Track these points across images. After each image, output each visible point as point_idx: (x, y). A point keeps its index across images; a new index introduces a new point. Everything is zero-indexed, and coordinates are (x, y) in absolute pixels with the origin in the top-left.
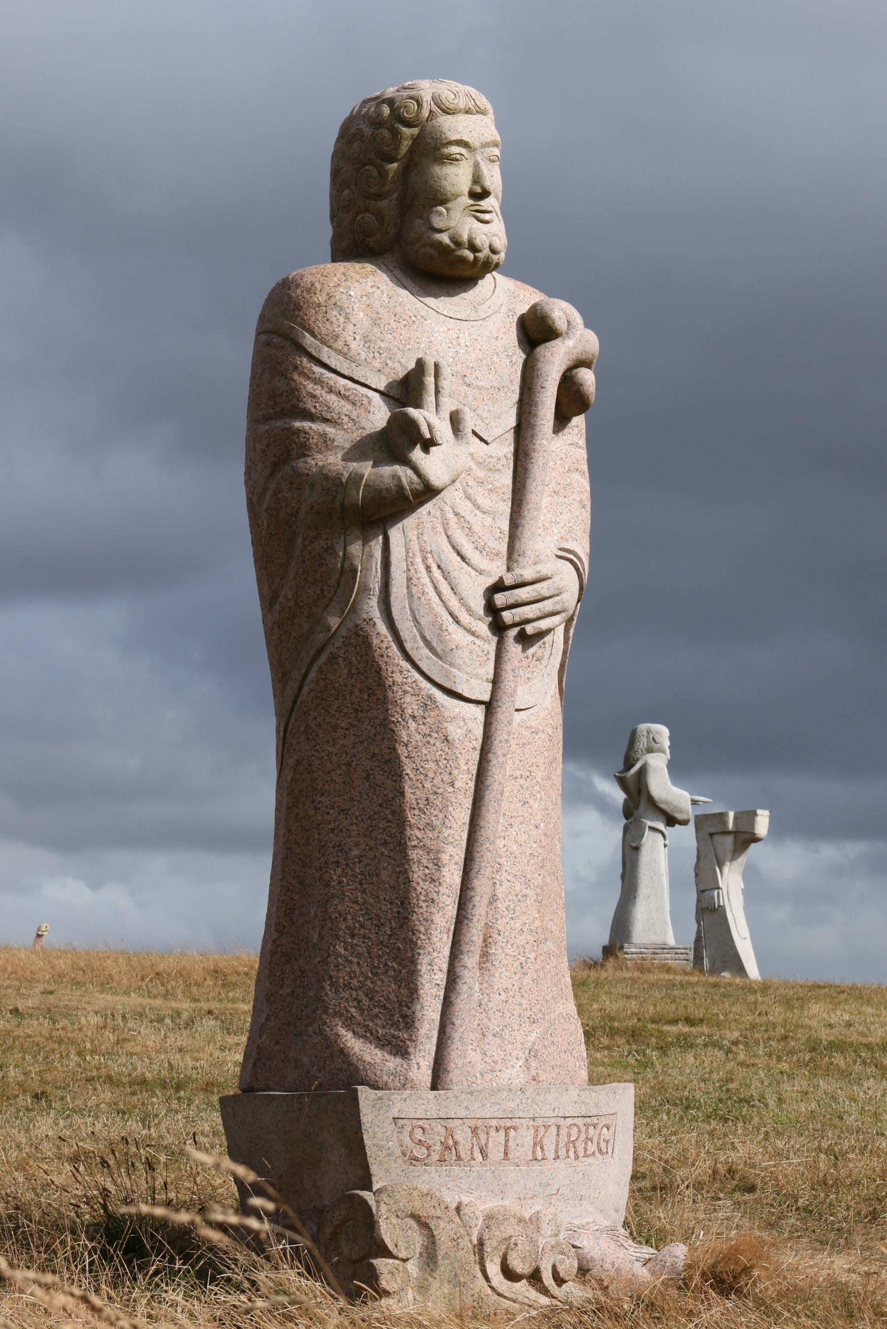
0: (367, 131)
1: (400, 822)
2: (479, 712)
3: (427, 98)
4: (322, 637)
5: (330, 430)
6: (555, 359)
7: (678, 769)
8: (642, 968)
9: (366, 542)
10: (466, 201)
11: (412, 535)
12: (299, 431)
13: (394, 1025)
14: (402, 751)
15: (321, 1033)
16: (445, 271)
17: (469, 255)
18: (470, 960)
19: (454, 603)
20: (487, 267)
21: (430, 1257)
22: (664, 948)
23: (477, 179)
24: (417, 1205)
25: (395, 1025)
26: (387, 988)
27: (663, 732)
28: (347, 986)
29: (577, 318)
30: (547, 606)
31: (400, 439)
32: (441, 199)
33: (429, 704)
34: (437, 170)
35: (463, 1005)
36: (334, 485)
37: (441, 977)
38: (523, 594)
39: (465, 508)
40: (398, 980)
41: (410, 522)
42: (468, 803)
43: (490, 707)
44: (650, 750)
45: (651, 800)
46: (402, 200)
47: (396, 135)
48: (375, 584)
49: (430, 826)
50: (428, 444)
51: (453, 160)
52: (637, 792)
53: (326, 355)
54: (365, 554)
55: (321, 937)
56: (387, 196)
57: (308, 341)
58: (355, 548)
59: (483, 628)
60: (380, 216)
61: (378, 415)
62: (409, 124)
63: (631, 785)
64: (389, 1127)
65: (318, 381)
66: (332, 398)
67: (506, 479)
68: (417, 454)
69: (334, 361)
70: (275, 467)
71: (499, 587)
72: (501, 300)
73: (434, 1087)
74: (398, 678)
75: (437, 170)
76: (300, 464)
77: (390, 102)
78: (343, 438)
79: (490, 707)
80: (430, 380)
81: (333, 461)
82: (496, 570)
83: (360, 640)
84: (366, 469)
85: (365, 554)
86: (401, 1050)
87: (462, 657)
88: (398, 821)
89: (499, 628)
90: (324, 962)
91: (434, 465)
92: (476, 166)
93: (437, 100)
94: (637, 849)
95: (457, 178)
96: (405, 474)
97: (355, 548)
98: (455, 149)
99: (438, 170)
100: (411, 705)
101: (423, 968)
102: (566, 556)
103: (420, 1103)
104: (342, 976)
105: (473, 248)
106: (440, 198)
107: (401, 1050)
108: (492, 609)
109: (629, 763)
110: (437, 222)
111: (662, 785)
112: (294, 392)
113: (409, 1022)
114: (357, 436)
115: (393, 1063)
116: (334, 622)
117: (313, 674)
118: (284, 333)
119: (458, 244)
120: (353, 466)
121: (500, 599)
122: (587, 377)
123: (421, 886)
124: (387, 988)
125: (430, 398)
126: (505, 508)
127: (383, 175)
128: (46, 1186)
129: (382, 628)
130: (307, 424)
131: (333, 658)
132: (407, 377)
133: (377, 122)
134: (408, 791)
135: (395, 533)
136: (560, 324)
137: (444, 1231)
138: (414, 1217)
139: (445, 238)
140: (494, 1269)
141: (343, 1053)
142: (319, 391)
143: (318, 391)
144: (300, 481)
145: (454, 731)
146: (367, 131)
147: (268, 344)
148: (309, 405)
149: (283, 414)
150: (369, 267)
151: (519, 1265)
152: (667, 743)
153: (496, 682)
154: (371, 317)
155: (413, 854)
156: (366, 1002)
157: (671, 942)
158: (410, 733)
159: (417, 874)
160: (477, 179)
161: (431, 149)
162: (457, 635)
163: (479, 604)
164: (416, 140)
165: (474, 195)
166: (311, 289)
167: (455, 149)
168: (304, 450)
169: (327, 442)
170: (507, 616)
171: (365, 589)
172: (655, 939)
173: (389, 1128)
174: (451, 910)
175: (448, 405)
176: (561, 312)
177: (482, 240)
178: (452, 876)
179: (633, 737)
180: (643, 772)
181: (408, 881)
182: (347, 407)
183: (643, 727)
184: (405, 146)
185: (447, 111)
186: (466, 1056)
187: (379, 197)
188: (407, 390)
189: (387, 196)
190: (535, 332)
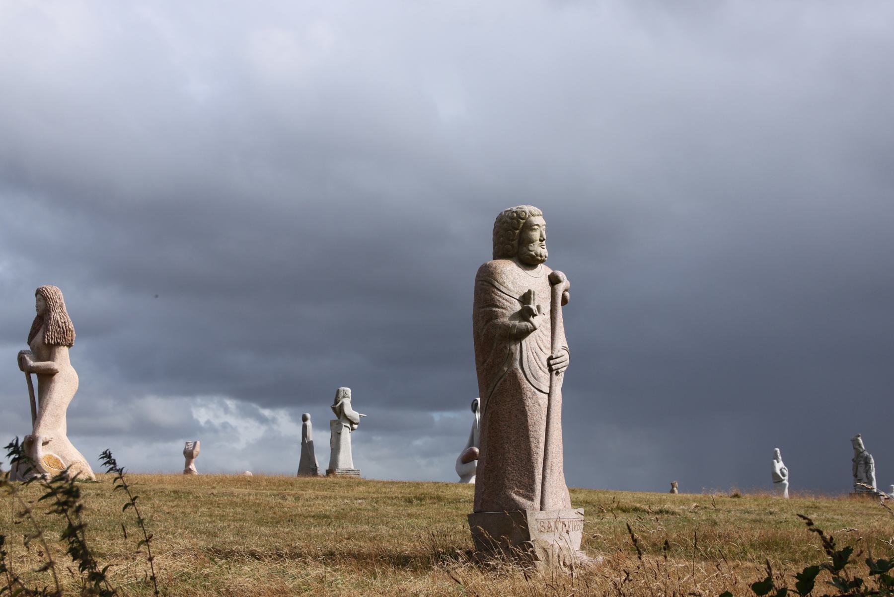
0: (509, 220)
2: (546, 396)
6: (560, 288)
8: (343, 477)
10: (538, 242)
13: (528, 491)
16: (529, 262)
18: (548, 471)
21: (547, 560)
22: (350, 470)
26: (526, 480)
27: (349, 391)
29: (565, 277)
30: (563, 364)
31: (526, 313)
32: (531, 241)
33: (534, 394)
35: (547, 485)
36: (507, 328)
37: (541, 477)
38: (558, 360)
39: (541, 335)
40: (529, 478)
41: (527, 339)
44: (344, 397)
45: (345, 416)
46: (519, 242)
47: (519, 222)
48: (518, 357)
49: (536, 431)
50: (534, 315)
52: (339, 411)
53: (502, 288)
54: (515, 348)
57: (496, 284)
58: (513, 347)
59: (547, 371)
60: (512, 246)
61: (518, 307)
62: (522, 219)
63: (337, 410)
65: (500, 296)
67: (549, 326)
68: (531, 319)
69: (504, 290)
70: (487, 322)
71: (551, 358)
72: (543, 271)
73: (541, 510)
77: (516, 212)
78: (508, 313)
81: (506, 320)
82: (549, 354)
83: (514, 375)
84: (517, 323)
85: (515, 348)
86: (532, 500)
87: (542, 380)
88: (527, 429)
89: (551, 370)
93: (530, 212)
94: (340, 434)
95: (536, 235)
96: (529, 324)
97: (513, 347)
99: (531, 233)
100: (529, 394)
102: (564, 348)
103: (541, 515)
104: (511, 477)
105: (541, 256)
107: (532, 500)
108: (549, 365)
109: (336, 402)
110: (531, 248)
111: (349, 410)
112: (493, 299)
113: (533, 490)
114: (512, 313)
115: (529, 503)
116: (506, 369)
117: (498, 385)
118: (486, 283)
121: (552, 362)
122: (567, 294)
123: (534, 449)
124: (526, 480)
126: (550, 334)
127: (514, 234)
128: (295, 548)
129: (520, 371)
131: (505, 380)
133: (512, 218)
135: (523, 342)
139: (533, 253)
141: (513, 500)
143: (501, 299)
144: (496, 326)
145: (541, 402)
146: (509, 220)
148: (497, 303)
149: (489, 306)
151: (568, 563)
152: (350, 395)
153: (551, 387)
154: (514, 278)
155: (532, 439)
157: (353, 468)
158: (529, 402)
159: (533, 445)
160: (541, 236)
161: (529, 226)
162: (541, 373)
163: (545, 364)
166: (496, 268)
168: (497, 317)
169: (503, 315)
172: (347, 467)
173: (535, 522)
175: (536, 304)
176: (561, 275)
177: (543, 254)
178: (542, 446)
179: (338, 392)
180: (342, 405)
183: (342, 388)
184: (521, 225)
185: (533, 215)
186: (549, 501)
187: (513, 240)
188: (526, 298)
189: (513, 239)
190: (554, 281)
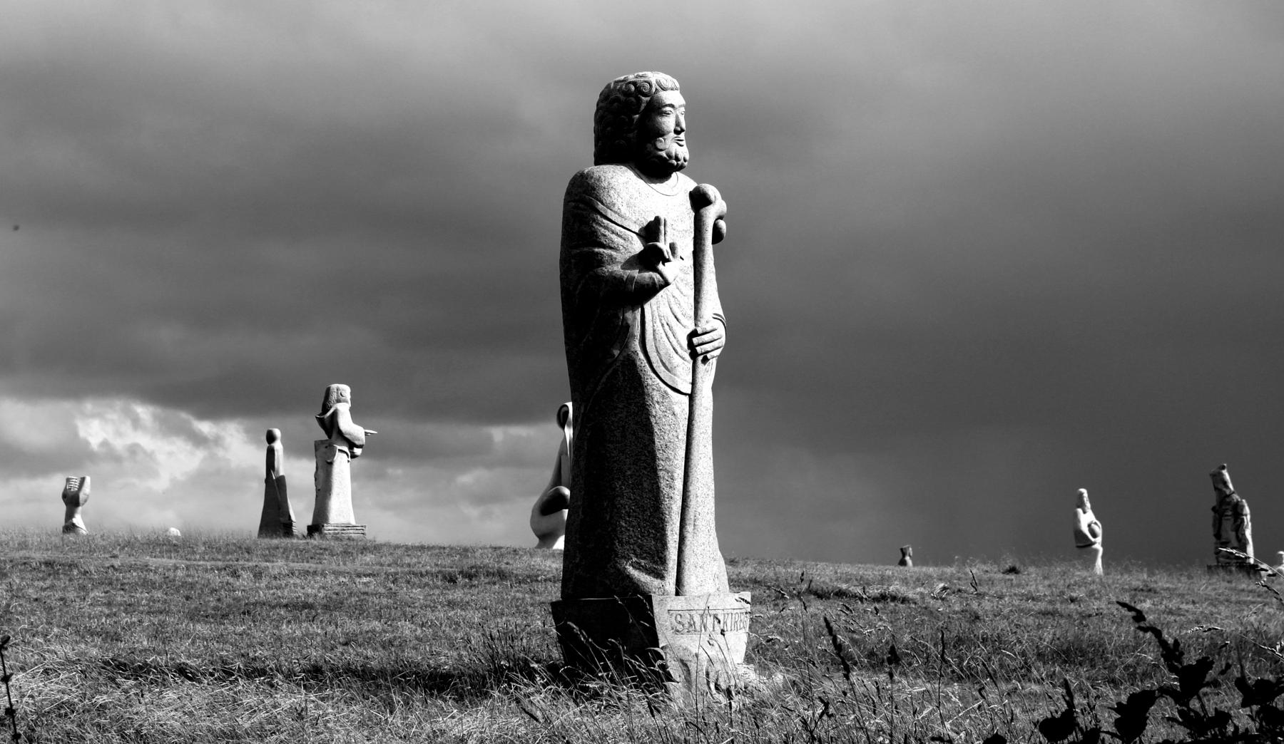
0: (622, 98)
1: (653, 457)
2: (686, 399)
3: (654, 82)
4: (610, 360)
5: (614, 253)
6: (710, 214)
7: (356, 414)
8: (337, 538)
9: (633, 311)
10: (672, 135)
11: (655, 308)
12: (598, 253)
14: (653, 420)
15: (615, 567)
17: (674, 162)
18: (689, 528)
19: (675, 343)
20: (679, 168)
21: (688, 681)
23: (678, 124)
24: (681, 654)
25: (655, 562)
27: (346, 390)
28: (628, 543)
31: (651, 257)
33: (665, 395)
34: (660, 119)
35: (688, 551)
36: (617, 281)
37: (677, 537)
39: (677, 293)
41: (653, 301)
42: (684, 446)
43: (691, 397)
44: (338, 401)
45: (340, 433)
48: (637, 332)
50: (666, 260)
51: (667, 114)
52: (330, 426)
53: (610, 214)
54: (633, 317)
55: (611, 517)
56: (628, 129)
57: (600, 206)
58: (629, 315)
59: (688, 358)
61: (637, 246)
62: (646, 95)
63: (327, 422)
64: (666, 615)
65: (606, 228)
66: (614, 236)
68: (660, 266)
71: (694, 334)
72: (681, 184)
73: (677, 594)
74: (650, 382)
75: (660, 119)
76: (599, 270)
77: (634, 83)
78: (621, 257)
79: (691, 397)
80: (662, 228)
81: (617, 269)
83: (631, 363)
84: (635, 273)
85: (633, 317)
86: (660, 576)
87: (679, 371)
89: (694, 355)
90: (614, 530)
91: (667, 269)
92: (677, 117)
93: (659, 83)
95: (668, 123)
96: (656, 276)
97: (629, 315)
98: (668, 109)
101: (669, 533)
102: (716, 317)
104: (625, 538)
105: (677, 159)
106: (661, 133)
107: (660, 576)
108: (691, 346)
109: (326, 408)
110: (660, 145)
111: (346, 423)
112: (594, 233)
113: (663, 561)
114: (627, 256)
115: (657, 582)
116: (616, 353)
118: (583, 203)
119: (670, 157)
120: (628, 272)
121: (695, 340)
122: (722, 224)
123: (666, 490)
125: (662, 237)
129: (641, 356)
130: (601, 250)
131: (615, 371)
132: (650, 224)
133: (627, 93)
134: (657, 440)
135: (647, 307)
136: (712, 198)
137: (693, 667)
138: (682, 661)
139: (664, 154)
140: (712, 686)
141: (629, 577)
142: (607, 233)
145: (677, 409)
147: (577, 207)
148: (603, 240)
150: (624, 168)
151: (724, 686)
153: (693, 383)
154: (630, 197)
155: (661, 474)
156: (638, 551)
157: (353, 523)
158: (656, 410)
159: (663, 484)
160: (678, 124)
161: (656, 108)
162: (676, 360)
163: (685, 343)
164: (649, 103)
165: (677, 132)
166: (599, 179)
167: (668, 109)
169: (612, 260)
170: (698, 349)
171: (633, 336)
174: (679, 503)
175: (669, 241)
176: (712, 191)
177: (681, 156)
178: (679, 484)
180: (335, 414)
181: (658, 488)
182: (621, 241)
183: (334, 386)
185: (664, 89)
186: (691, 580)
188: (651, 231)
189: (628, 129)
190: (699, 200)
